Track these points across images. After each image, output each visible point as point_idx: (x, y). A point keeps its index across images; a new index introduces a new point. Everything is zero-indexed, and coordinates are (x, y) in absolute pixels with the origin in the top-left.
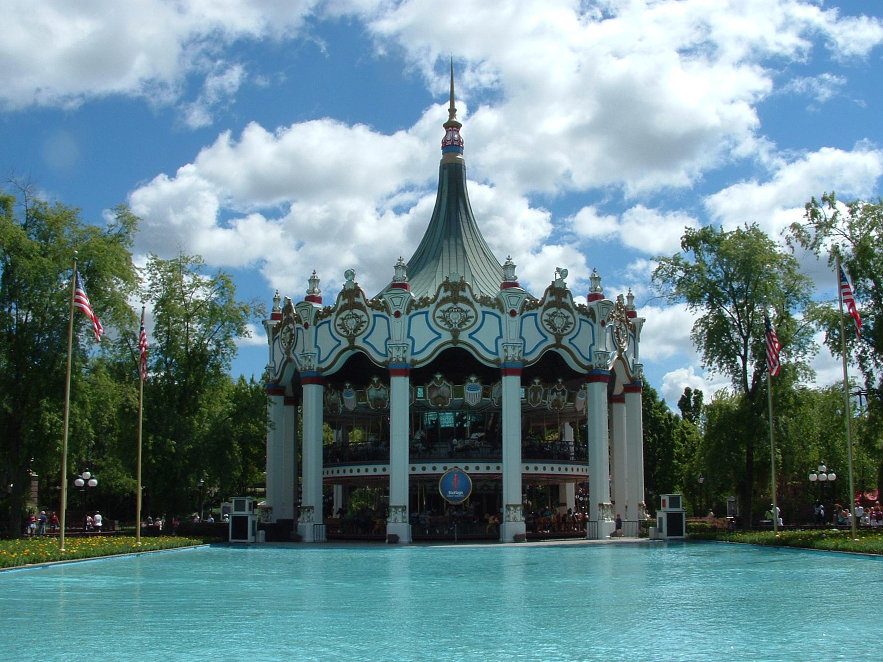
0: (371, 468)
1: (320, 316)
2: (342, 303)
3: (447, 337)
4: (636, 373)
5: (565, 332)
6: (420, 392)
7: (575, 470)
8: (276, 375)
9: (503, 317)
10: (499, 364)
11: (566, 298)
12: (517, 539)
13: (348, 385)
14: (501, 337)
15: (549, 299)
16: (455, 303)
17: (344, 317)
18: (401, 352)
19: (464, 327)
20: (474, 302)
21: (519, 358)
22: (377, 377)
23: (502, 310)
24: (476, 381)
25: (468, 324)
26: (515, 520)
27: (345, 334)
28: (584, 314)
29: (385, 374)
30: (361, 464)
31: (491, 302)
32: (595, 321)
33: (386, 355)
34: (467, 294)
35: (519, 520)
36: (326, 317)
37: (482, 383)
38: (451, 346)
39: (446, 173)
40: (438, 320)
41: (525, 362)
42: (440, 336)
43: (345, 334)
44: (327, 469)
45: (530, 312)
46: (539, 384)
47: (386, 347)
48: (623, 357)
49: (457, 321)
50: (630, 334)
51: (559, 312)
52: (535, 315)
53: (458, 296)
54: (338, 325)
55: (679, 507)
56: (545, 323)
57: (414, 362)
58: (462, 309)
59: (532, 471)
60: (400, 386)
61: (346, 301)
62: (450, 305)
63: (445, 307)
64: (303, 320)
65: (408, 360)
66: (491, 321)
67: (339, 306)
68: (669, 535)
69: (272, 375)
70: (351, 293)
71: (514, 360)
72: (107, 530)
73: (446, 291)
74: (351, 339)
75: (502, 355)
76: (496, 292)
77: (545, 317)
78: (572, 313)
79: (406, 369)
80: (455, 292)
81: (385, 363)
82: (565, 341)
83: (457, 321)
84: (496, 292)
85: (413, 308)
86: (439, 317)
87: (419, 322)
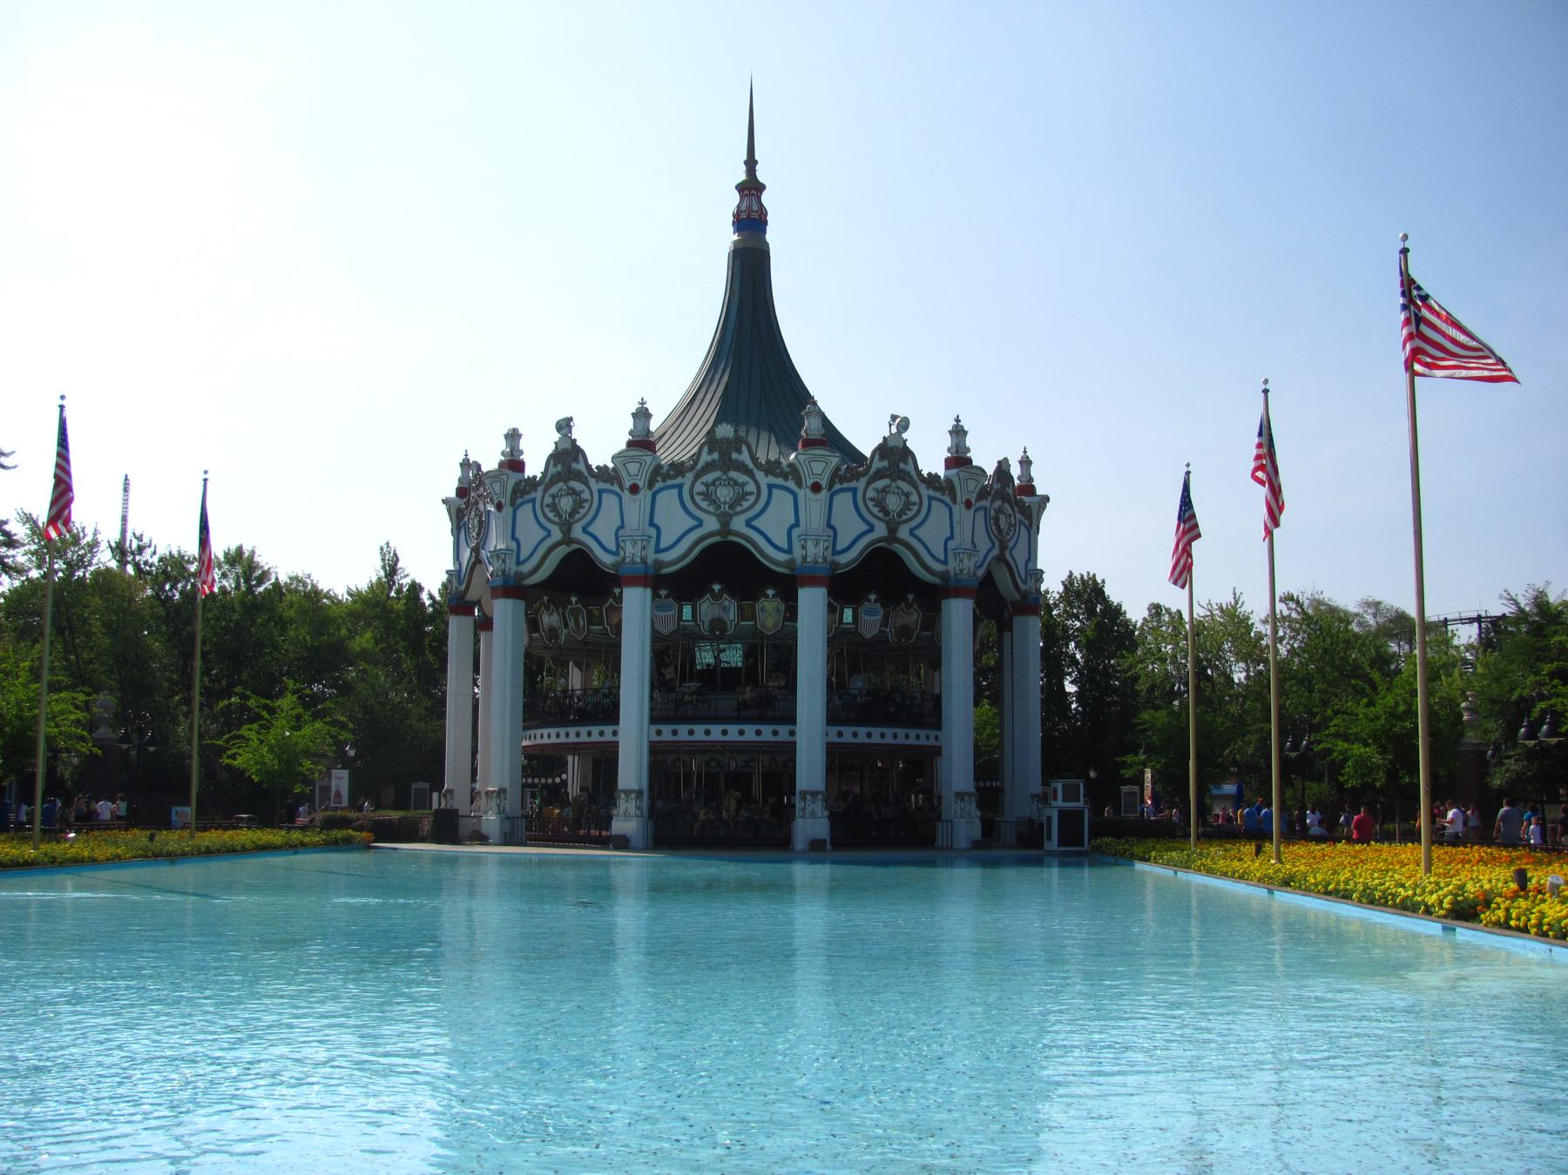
0: (862, 738)
2: (705, 458)
3: (711, 524)
4: (1031, 584)
5: (904, 517)
6: (848, 615)
7: (545, 736)
8: (460, 583)
9: (801, 493)
10: (793, 569)
12: (816, 846)
13: (872, 597)
14: (797, 524)
15: (997, 486)
16: (725, 472)
17: (555, 492)
18: (639, 548)
19: (904, 517)
20: (755, 470)
21: (825, 558)
22: (720, 584)
23: (799, 484)
25: (746, 504)
26: (813, 814)
29: (788, 585)
30: (921, 728)
31: (782, 470)
32: (954, 500)
33: (616, 554)
34: (745, 457)
35: (819, 815)
36: (528, 493)
41: (835, 565)
42: (700, 524)
43: (556, 519)
44: (612, 738)
45: (845, 485)
46: (576, 603)
47: (617, 539)
48: (1008, 557)
50: (1020, 521)
51: (894, 485)
52: (854, 491)
54: (547, 506)
55: (1078, 801)
56: (870, 504)
57: (659, 564)
59: (848, 738)
60: (812, 603)
61: (559, 468)
62: (717, 474)
63: (709, 477)
64: (495, 497)
65: (650, 561)
66: (939, 511)
67: (549, 476)
68: (1060, 844)
69: (455, 583)
70: (567, 455)
71: (817, 562)
72: (128, 822)
74: (566, 527)
75: (798, 553)
76: (662, 457)
77: (993, 514)
79: (646, 576)
80: (725, 455)
81: (617, 565)
82: (903, 532)
83: (728, 500)
84: (662, 457)
86: (699, 494)
87: (668, 500)
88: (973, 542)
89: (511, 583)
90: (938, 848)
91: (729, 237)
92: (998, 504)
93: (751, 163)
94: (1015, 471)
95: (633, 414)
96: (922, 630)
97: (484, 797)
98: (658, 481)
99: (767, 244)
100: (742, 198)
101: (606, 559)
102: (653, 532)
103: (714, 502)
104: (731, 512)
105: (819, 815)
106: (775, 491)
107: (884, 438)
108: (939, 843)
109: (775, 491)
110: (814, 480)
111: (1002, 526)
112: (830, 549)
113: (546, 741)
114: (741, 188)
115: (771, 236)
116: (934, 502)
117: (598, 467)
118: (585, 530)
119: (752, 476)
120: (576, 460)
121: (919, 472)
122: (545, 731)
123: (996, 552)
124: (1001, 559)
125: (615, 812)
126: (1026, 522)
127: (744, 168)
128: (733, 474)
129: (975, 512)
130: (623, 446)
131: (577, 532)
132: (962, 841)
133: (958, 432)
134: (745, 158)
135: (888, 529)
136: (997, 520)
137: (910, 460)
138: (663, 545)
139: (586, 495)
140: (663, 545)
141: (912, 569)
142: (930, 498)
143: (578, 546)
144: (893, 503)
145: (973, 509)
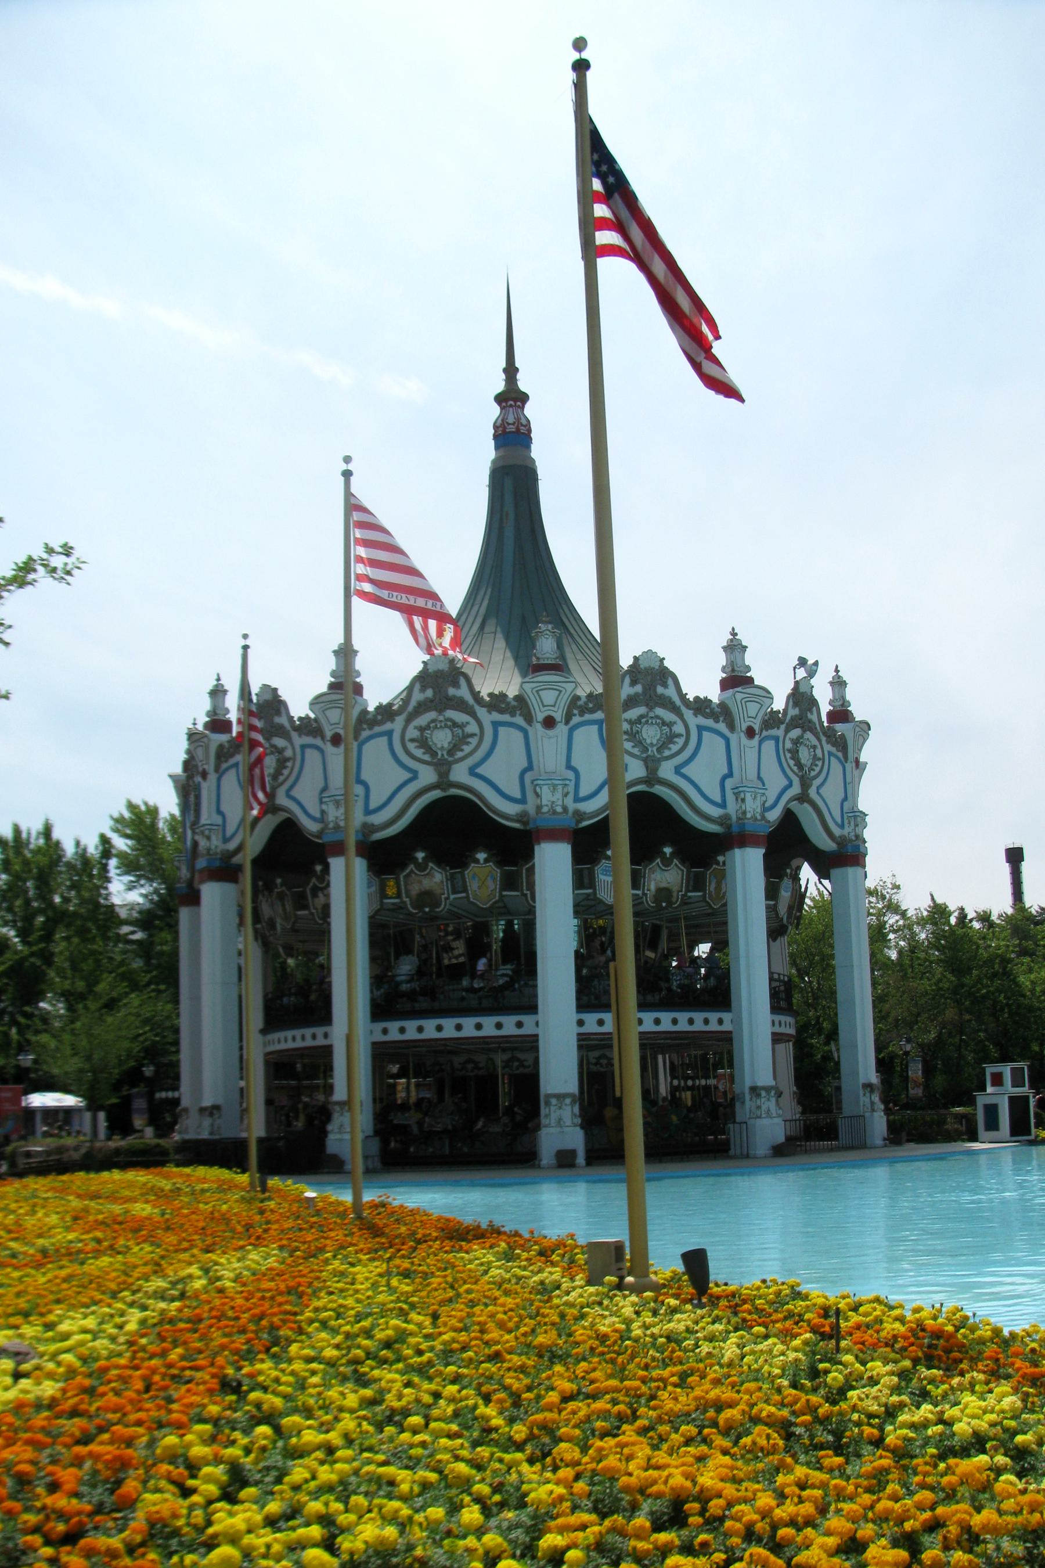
1: (367, 722)
2: (417, 696)
7: (299, 1038)
9: (733, 738)
11: (812, 713)
14: (730, 774)
15: (793, 712)
18: (559, 795)
20: (477, 708)
23: (732, 727)
24: (486, 861)
25: (467, 749)
26: (769, 1114)
27: (427, 757)
28: (833, 745)
32: (732, 727)
37: (500, 863)
38: (436, 794)
39: (509, 483)
40: (411, 746)
41: (579, 815)
49: (655, 742)
53: (656, 695)
55: (1013, 1086)
56: (788, 755)
58: (662, 719)
59: (394, 1035)
63: (423, 720)
66: (713, 745)
67: (413, 703)
73: (633, 683)
75: (732, 808)
77: (789, 745)
78: (680, 715)
81: (320, 834)
83: (655, 742)
85: (576, 712)
86: (412, 740)
88: (759, 778)
89: (218, 864)
90: (735, 1157)
91: (487, 452)
92: (795, 733)
93: (511, 371)
94: (823, 695)
95: (335, 652)
96: (687, 891)
97: (194, 1114)
98: (364, 730)
99: (533, 461)
100: (502, 409)
101: (311, 826)
102: (571, 775)
103: (640, 743)
104: (450, 759)
105: (568, 1122)
106: (501, 729)
107: (635, 657)
108: (732, 1152)
109: (501, 729)
110: (546, 714)
111: (803, 761)
112: (571, 796)
113: (291, 1045)
114: (500, 399)
115: (537, 452)
116: (705, 734)
117: (300, 719)
118: (289, 796)
119: (473, 714)
120: (278, 713)
121: (683, 697)
122: (289, 1034)
123: (796, 789)
124: (803, 798)
125: (329, 1127)
126: (840, 754)
127: (504, 377)
128: (451, 714)
129: (760, 743)
130: (324, 689)
131: (281, 800)
132: (762, 1148)
133: (734, 647)
134: (504, 365)
135: (647, 768)
136: (794, 753)
137: (670, 682)
138: (373, 805)
139: (288, 753)
140: (373, 805)
141: (692, 823)
142: (700, 729)
143: (287, 815)
144: (651, 734)
145: (757, 737)
